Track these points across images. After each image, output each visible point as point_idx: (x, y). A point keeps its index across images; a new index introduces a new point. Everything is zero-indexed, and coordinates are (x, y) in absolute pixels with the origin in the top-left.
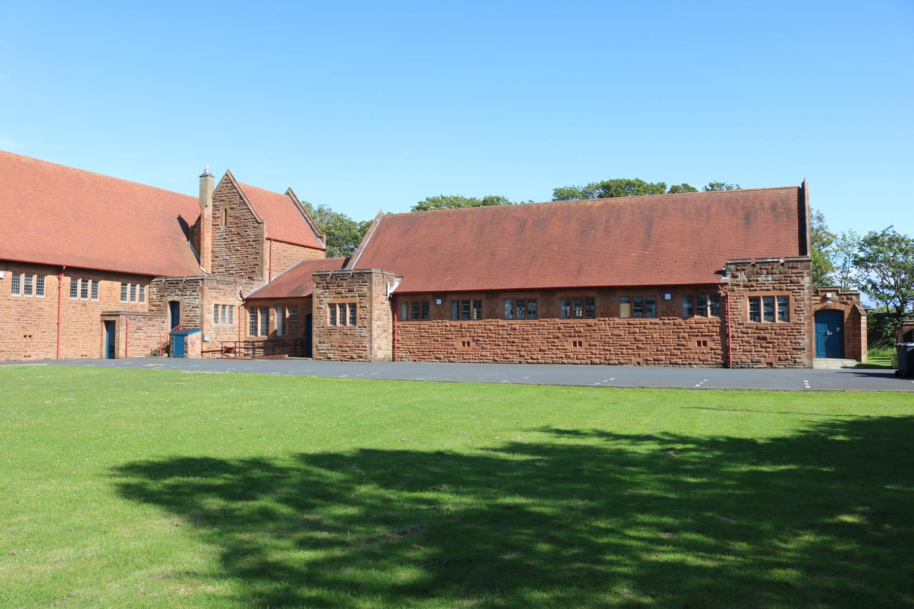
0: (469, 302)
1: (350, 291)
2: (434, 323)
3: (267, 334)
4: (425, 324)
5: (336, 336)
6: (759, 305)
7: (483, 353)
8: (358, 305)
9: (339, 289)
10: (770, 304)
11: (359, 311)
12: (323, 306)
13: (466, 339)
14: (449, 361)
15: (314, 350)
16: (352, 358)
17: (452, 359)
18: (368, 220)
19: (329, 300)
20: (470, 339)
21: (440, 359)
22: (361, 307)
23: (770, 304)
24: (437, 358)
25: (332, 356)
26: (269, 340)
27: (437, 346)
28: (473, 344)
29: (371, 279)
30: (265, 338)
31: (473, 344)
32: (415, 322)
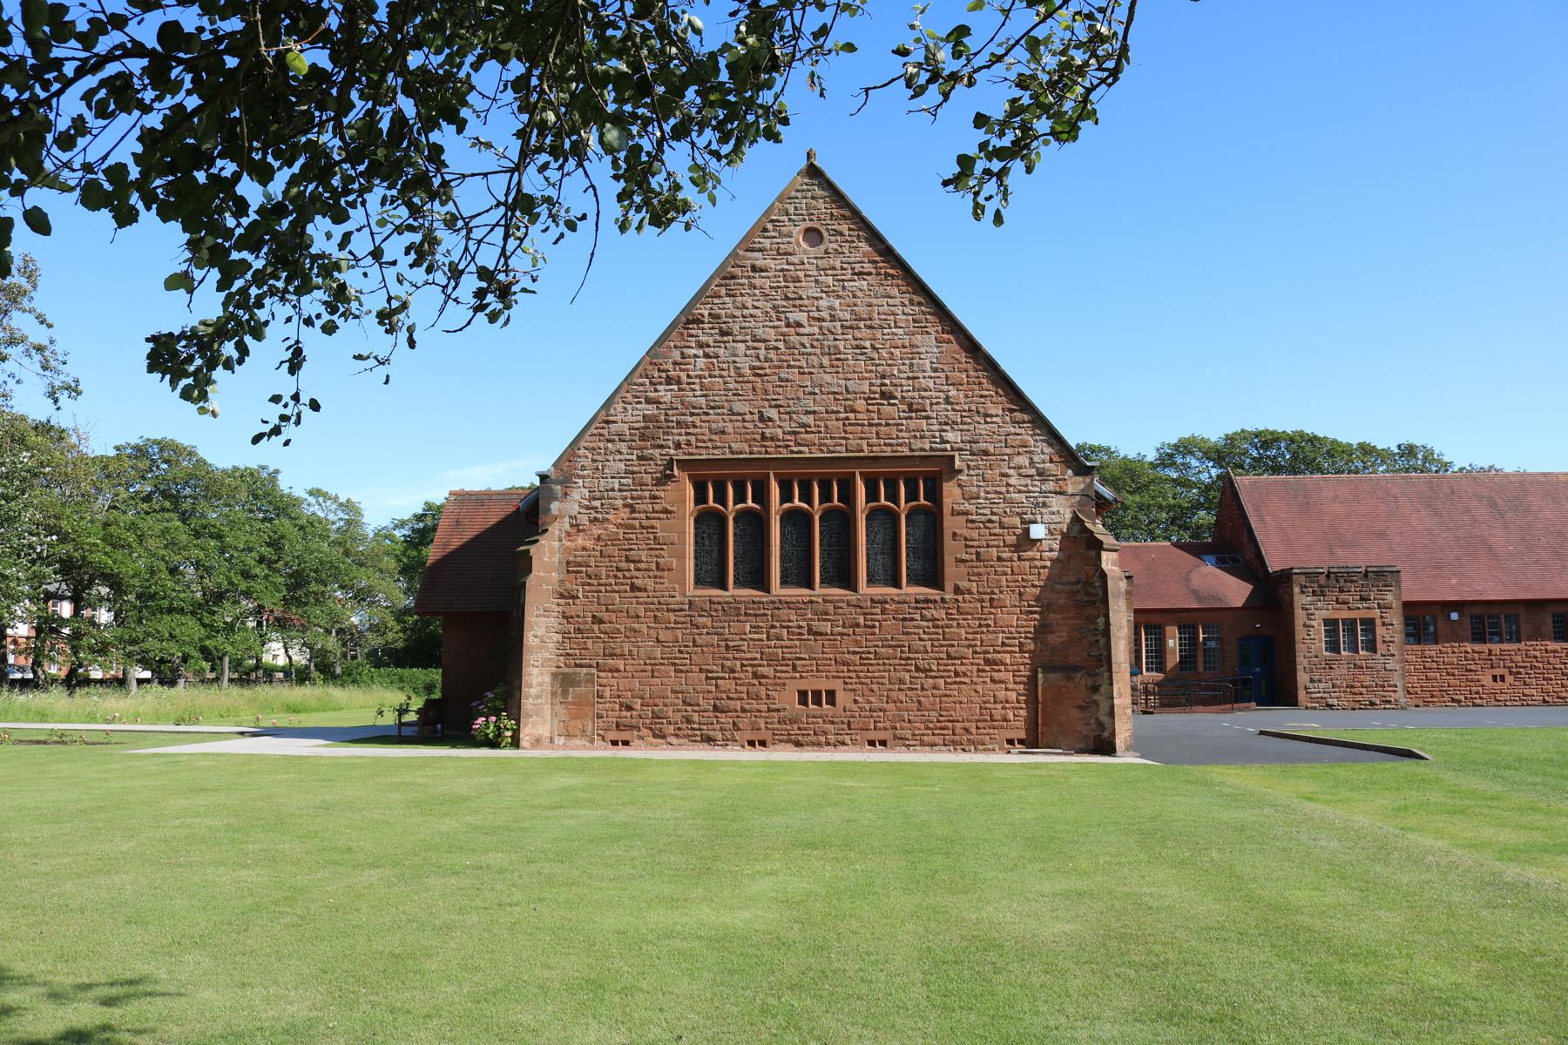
0: (1498, 617)
1: (1362, 599)
2: (1447, 647)
3: (1160, 667)
4: (1432, 650)
5: (1341, 671)
6: (1336, 631)
7: (1527, 692)
8: (1378, 622)
9: (1342, 597)
10: (1351, 631)
11: (1380, 631)
12: (1314, 623)
13: (1498, 672)
14: (1474, 705)
15: (1302, 695)
16: (1372, 704)
17: (1478, 701)
18: (514, 472)
19: (1325, 614)
20: (1506, 672)
21: (1459, 701)
22: (1384, 624)
23: (1351, 631)
24: (1453, 700)
25: (1335, 702)
26: (1166, 679)
27: (1453, 682)
28: (1509, 679)
29: (1398, 582)
30: (1159, 676)
31: (1509, 679)
32: (1415, 647)
